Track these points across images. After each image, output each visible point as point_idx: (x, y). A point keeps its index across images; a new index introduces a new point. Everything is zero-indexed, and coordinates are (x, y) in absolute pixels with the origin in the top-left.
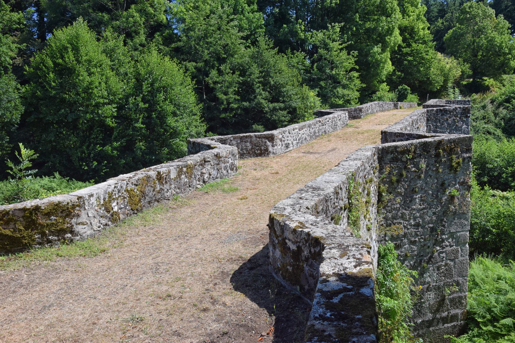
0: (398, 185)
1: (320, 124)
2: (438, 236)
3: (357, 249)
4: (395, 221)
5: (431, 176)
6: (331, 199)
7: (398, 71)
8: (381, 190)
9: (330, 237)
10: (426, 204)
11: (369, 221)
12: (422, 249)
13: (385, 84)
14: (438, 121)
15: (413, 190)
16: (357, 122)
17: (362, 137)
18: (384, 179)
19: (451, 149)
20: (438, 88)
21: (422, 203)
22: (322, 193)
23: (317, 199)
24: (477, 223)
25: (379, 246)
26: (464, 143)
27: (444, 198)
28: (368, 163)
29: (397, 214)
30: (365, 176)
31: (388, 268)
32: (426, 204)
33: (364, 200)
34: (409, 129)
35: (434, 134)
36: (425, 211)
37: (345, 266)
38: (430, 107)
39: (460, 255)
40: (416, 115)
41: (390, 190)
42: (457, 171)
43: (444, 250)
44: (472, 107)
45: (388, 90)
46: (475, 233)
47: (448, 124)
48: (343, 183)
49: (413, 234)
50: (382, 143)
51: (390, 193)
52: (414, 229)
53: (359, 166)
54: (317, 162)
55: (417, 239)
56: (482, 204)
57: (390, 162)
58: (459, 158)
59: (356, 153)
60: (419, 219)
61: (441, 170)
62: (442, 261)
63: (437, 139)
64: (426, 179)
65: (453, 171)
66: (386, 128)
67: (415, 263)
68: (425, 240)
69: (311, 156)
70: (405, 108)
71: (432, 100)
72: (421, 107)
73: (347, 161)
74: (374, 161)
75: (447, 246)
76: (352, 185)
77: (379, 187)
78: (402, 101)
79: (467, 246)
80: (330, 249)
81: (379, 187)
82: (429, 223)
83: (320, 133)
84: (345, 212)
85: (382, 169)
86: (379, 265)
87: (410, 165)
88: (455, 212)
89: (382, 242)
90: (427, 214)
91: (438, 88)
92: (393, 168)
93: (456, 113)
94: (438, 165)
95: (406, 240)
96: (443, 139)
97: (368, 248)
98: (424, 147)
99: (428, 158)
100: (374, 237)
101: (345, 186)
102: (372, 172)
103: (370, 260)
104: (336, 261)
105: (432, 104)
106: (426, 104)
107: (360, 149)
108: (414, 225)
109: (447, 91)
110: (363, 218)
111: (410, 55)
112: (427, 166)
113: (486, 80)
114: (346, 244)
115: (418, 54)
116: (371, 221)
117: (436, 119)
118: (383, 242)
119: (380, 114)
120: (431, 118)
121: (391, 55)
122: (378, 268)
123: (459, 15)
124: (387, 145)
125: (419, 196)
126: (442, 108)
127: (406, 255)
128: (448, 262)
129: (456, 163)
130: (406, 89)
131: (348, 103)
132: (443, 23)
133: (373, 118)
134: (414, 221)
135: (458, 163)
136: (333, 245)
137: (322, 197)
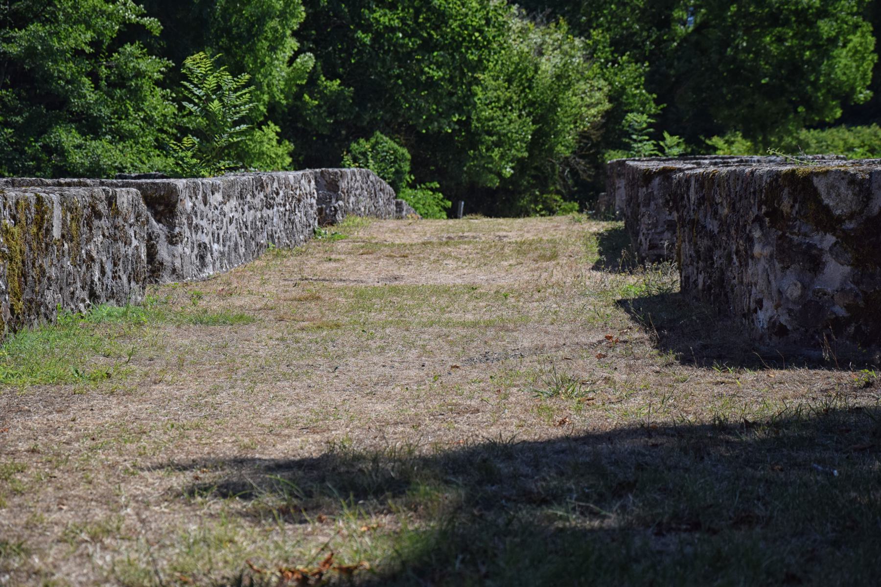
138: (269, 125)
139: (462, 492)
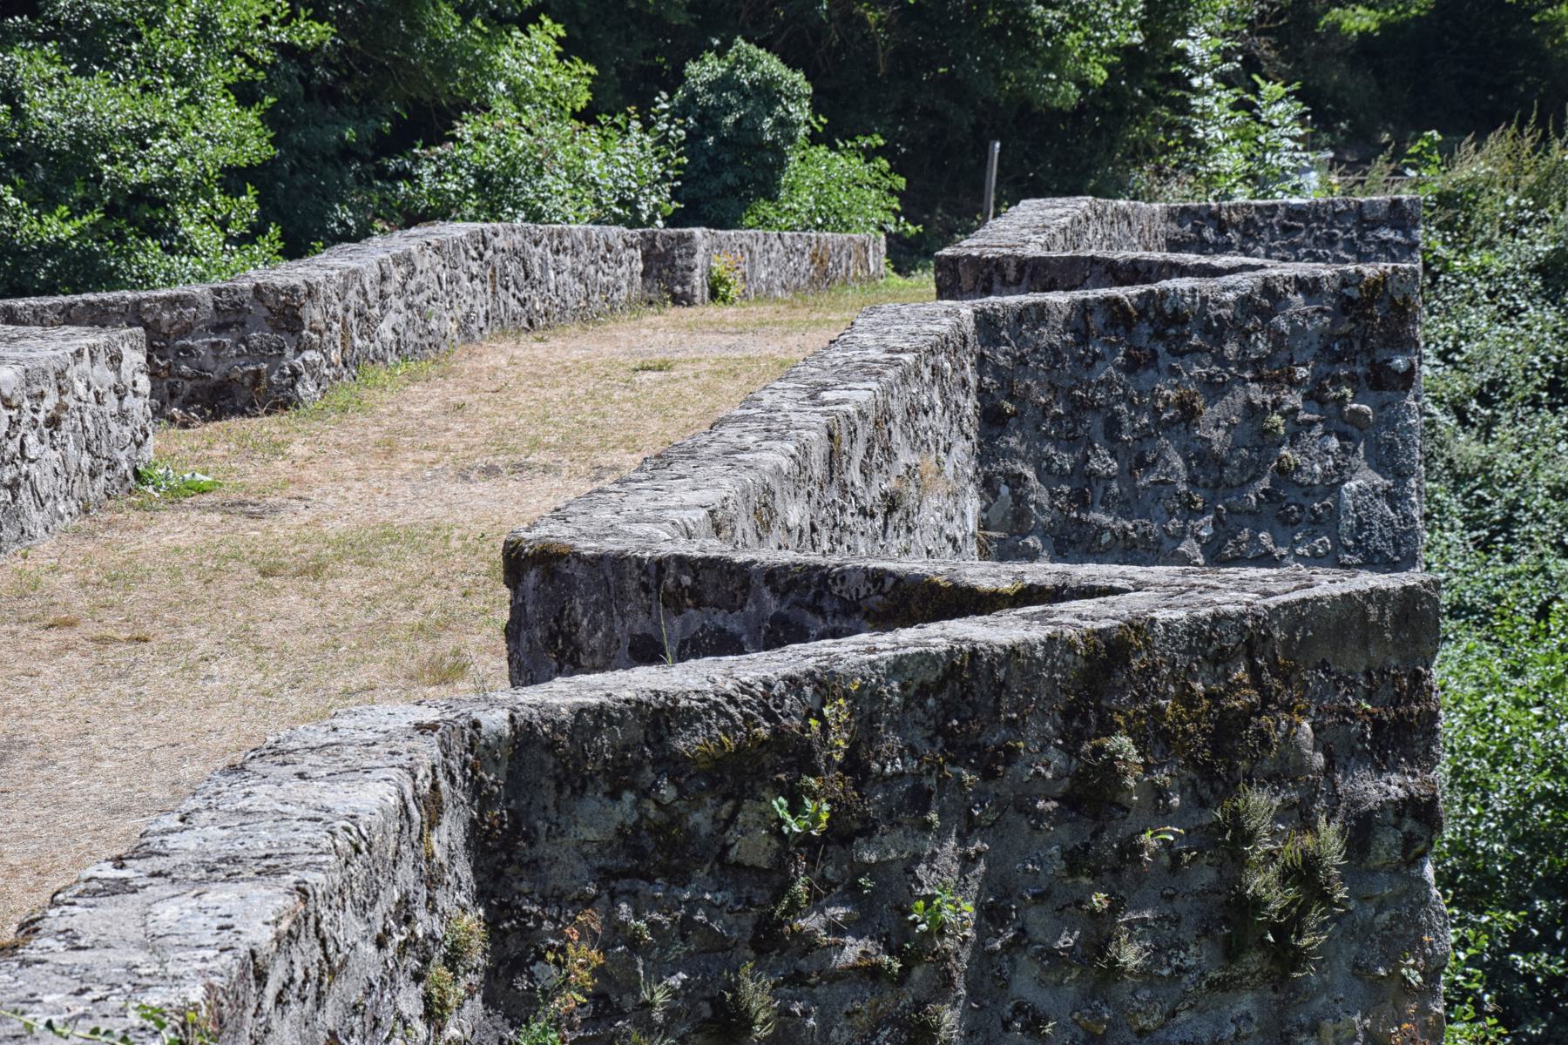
14: (1094, 423)
16: (247, 449)
17: (307, 611)
20: (1099, 75)
26: (1354, 661)
28: (363, 908)
34: (795, 513)
35: (1043, 572)
40: (867, 370)
42: (1299, 958)
44: (1434, 270)
45: (583, 98)
47: (1202, 459)
50: (524, 672)
53: (263, 937)
57: (605, 876)
58: (1307, 824)
59: (234, 795)
61: (1130, 955)
65: (1253, 960)
66: (560, 515)
70: (764, 296)
71: (1029, 210)
72: (925, 280)
73: (121, 887)
74: (432, 881)
78: (722, 222)
87: (816, 901)
92: (634, 942)
93: (1277, 338)
94: (1099, 900)
96: (1140, 627)
98: (948, 710)
99: (992, 829)
102: (410, 1001)
105: (1033, 250)
106: (970, 246)
107: (278, 753)
109: (1183, 107)
112: (991, 915)
117: (1078, 408)
126: (1127, 293)
129: (1285, 876)
130: (767, 93)
131: (152, 230)
135: (1305, 874)
138: (542, 24)
139: (1342, 65)
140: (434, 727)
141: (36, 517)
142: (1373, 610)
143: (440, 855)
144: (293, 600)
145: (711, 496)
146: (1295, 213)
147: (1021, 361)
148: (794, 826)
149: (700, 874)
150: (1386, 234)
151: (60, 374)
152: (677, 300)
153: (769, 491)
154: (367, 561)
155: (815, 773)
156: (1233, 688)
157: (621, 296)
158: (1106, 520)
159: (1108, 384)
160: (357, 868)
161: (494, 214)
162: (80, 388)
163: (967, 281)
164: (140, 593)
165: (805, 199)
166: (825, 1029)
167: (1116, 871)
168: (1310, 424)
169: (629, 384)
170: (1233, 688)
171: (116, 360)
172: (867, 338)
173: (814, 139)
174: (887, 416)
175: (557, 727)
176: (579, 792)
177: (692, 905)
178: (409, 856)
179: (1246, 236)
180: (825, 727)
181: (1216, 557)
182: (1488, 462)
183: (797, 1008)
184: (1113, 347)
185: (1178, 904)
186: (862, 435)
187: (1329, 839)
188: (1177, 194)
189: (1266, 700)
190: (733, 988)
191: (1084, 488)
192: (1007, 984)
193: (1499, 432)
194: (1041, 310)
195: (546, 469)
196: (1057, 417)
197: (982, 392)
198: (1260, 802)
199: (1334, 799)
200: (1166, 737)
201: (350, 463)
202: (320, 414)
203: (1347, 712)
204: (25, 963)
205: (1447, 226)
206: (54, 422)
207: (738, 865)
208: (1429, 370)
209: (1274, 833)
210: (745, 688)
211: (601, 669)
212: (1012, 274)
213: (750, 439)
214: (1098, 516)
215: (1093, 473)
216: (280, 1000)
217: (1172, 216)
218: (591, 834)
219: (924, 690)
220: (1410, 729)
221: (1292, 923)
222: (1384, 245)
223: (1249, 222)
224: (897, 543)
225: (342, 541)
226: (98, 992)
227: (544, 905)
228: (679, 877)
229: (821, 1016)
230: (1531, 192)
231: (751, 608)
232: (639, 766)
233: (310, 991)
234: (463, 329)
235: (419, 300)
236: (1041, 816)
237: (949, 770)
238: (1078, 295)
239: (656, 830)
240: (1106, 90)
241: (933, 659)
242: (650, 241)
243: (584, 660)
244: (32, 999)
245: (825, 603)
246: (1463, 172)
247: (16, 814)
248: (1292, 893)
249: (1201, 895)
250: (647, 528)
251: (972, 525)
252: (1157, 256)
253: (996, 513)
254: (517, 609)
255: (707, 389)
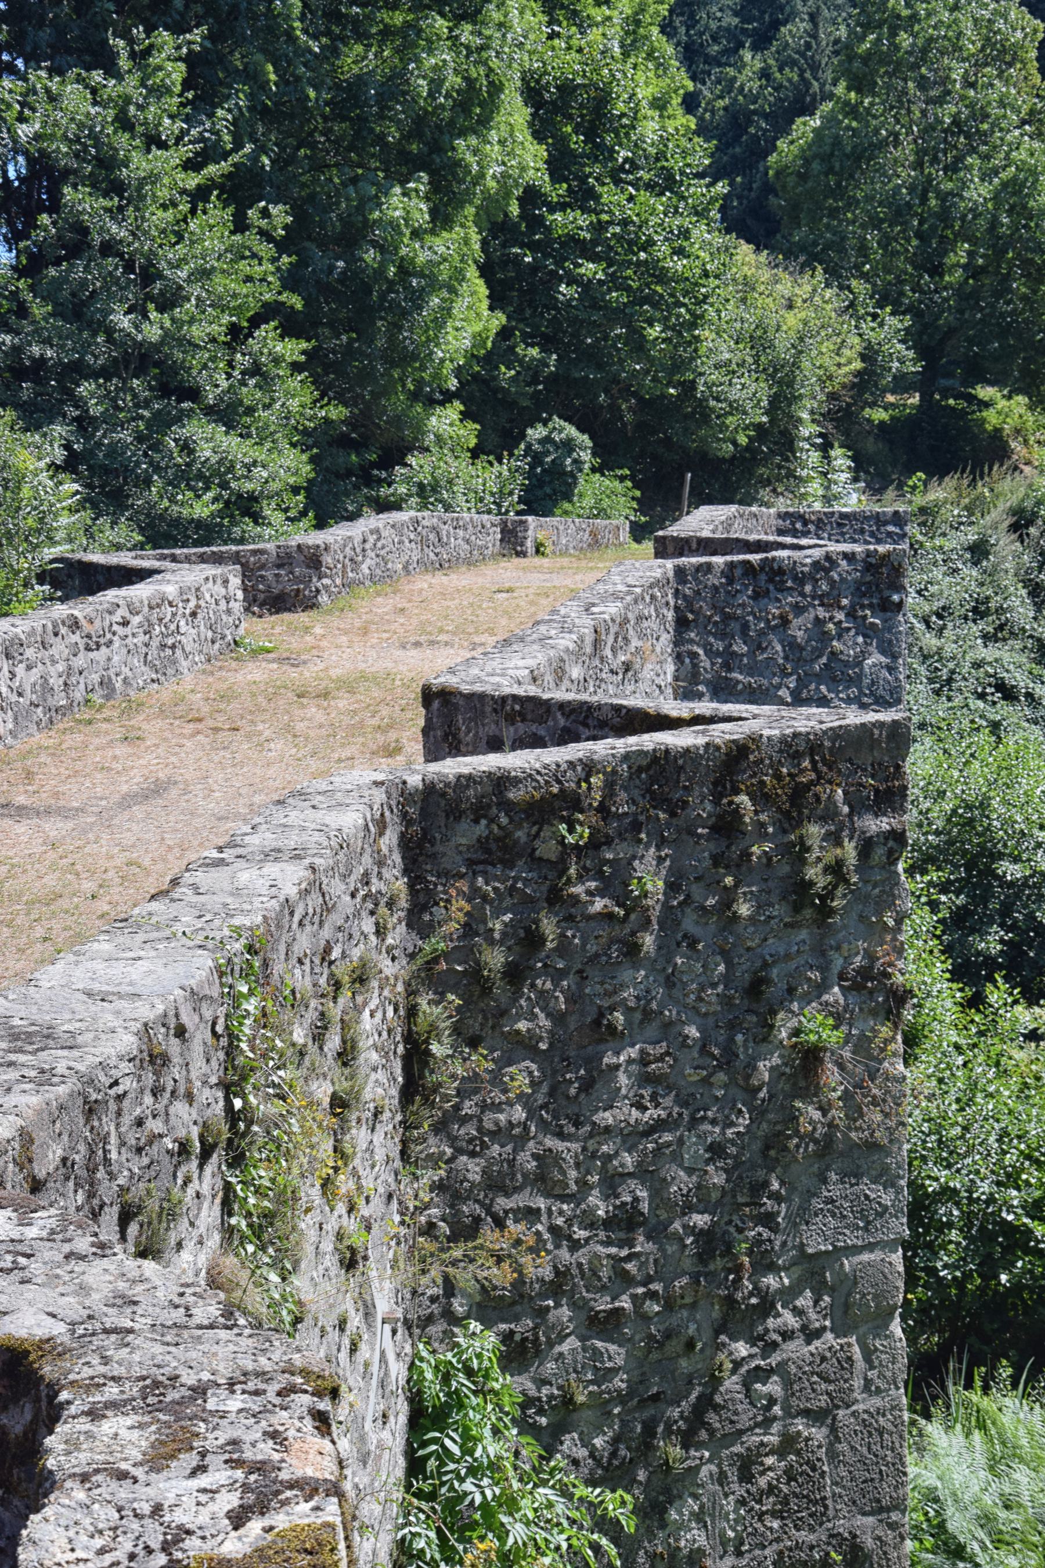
0: (517, 994)
1: (76, 638)
2: (739, 1279)
3: (255, 1404)
4: (502, 1203)
5: (693, 942)
6: (120, 1098)
7: (528, 340)
8: (421, 1024)
9: (96, 1342)
10: (668, 1101)
11: (351, 1209)
12: (655, 1356)
13: (453, 412)
14: (736, 627)
15: (597, 1023)
16: (292, 630)
17: (320, 717)
18: (435, 960)
19: (799, 792)
20: (743, 440)
21: (646, 1092)
22: (61, 1061)
23: (34, 1100)
24: (948, 1193)
25: (416, 1355)
26: (866, 759)
27: (764, 1069)
28: (344, 877)
29: (512, 1163)
30: (328, 950)
31: (468, 1486)
32: (668, 1101)
33: (322, 1091)
34: (576, 672)
35: (705, 707)
36: (667, 1137)
37: (179, 1517)
38: (693, 553)
39: (858, 1383)
40: (616, 596)
41: (474, 1026)
42: (831, 912)
43: (774, 1360)
45: (473, 442)
46: (943, 1246)
47: (792, 646)
48: (196, 998)
49: (605, 1273)
50: (432, 755)
51: (474, 1043)
52: (608, 1243)
53: (292, 891)
54: (53, 867)
55: (625, 1303)
56: (973, 1086)
57: (471, 863)
58: (839, 843)
59: (279, 816)
60: (633, 1183)
61: (744, 910)
62: (767, 1423)
63: (722, 733)
64: (669, 960)
65: (808, 913)
66: (452, 671)
67: (616, 1441)
68: (670, 1304)
69: (21, 828)
70: (565, 552)
71: (705, 512)
72: (648, 546)
73: (221, 863)
74: (381, 863)
75: (787, 1335)
76: (251, 1006)
77: (412, 1012)
78: (547, 513)
79: (896, 1328)
80: (94, 1414)
81: (412, 1012)
82: (688, 1208)
83: (78, 695)
84: (209, 1170)
85: (425, 908)
86: (415, 1466)
87: (581, 879)
88: (829, 1140)
89: (433, 1330)
90: (676, 1158)
91: (743, 440)
92: (485, 897)
93: (832, 583)
95: (565, 1312)
96: (755, 739)
97: (318, 1393)
100: (384, 1305)
101: (208, 1014)
102: (368, 925)
103: (327, 1470)
104: (123, 1492)
105: (706, 534)
106: (675, 530)
108: (608, 1223)
110: (316, 1192)
111: (586, 250)
112: (672, 887)
113: (987, 405)
114: (189, 1378)
115: (633, 245)
116: (365, 1211)
117: (727, 618)
118: (436, 1330)
119: (424, 583)
120: (696, 613)
121: (484, 243)
122: (408, 1487)
123: (851, 32)
124: (452, 767)
125: (633, 1052)
126: (755, 558)
127: (568, 1401)
128: (800, 1425)
129: (826, 870)
130: (568, 445)
132: (765, 74)
133: (383, 605)
134: (606, 1198)
136: (112, 1391)
137: (62, 1090)
140: (382, 783)
141: (184, 663)
142: (876, 732)
143: (385, 850)
144: (313, 711)
145: (532, 663)
146: (843, 516)
147: (698, 593)
148: (570, 839)
149: (520, 863)
150: (891, 528)
151: (198, 589)
152: (518, 554)
153: (562, 660)
154: (352, 692)
155: (582, 812)
156: (802, 771)
157: (489, 552)
158: (740, 677)
159: (743, 605)
160: (341, 856)
161: (424, 506)
162: (207, 596)
163: (670, 549)
164: (235, 705)
165: (588, 502)
166: (584, 945)
167: (738, 866)
168: (848, 629)
169: (491, 599)
170: (802, 771)
171: (226, 582)
172: (617, 579)
173: (594, 470)
174: (626, 620)
175: (447, 785)
176: (458, 819)
177: (516, 879)
178: (369, 850)
179: (818, 528)
180: (589, 788)
181: (798, 700)
182: (940, 649)
183: (569, 933)
184: (746, 586)
185: (770, 883)
186: (612, 631)
187: (850, 851)
188: (783, 504)
189: (820, 777)
190: (537, 922)
191: (730, 660)
192: (679, 924)
193: (946, 633)
194: (709, 566)
195: (446, 644)
196: (716, 623)
197: (677, 608)
198: (814, 831)
199: (853, 830)
200: (766, 797)
201: (344, 638)
202: (330, 612)
203: (861, 785)
204: (173, 900)
205: (923, 524)
206: (194, 614)
207: (540, 859)
208: (911, 600)
209: (821, 847)
210: (546, 766)
211: (473, 753)
212: (694, 546)
213: (553, 632)
214: (736, 675)
215: (734, 653)
216: (301, 924)
217: (780, 516)
218: (464, 841)
219: (640, 770)
220: (893, 794)
221: (829, 894)
222: (889, 534)
223: (820, 520)
224: (629, 688)
225: (339, 680)
226: (208, 917)
227: (439, 877)
228: (509, 864)
229: (582, 938)
230: (966, 508)
231: (551, 723)
232: (489, 806)
233: (316, 919)
234: (405, 568)
235: (383, 552)
236: (700, 836)
237: (652, 812)
238: (729, 558)
239: (498, 839)
240: (747, 448)
241: (646, 753)
242: (504, 523)
243: (463, 749)
244: (176, 919)
245: (590, 721)
246: (931, 496)
247: (172, 818)
248: (829, 878)
249: (782, 879)
250: (496, 679)
251: (670, 678)
252: (771, 538)
253: (682, 674)
254: (428, 720)
255: (532, 603)
